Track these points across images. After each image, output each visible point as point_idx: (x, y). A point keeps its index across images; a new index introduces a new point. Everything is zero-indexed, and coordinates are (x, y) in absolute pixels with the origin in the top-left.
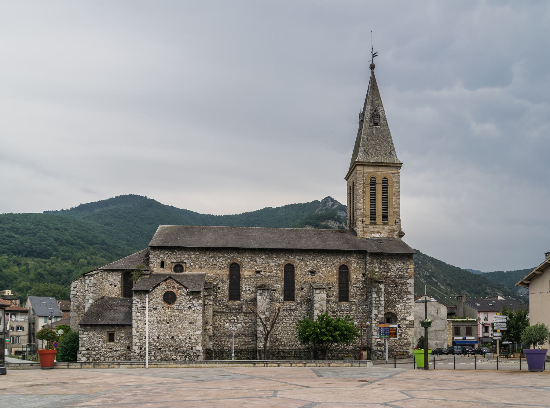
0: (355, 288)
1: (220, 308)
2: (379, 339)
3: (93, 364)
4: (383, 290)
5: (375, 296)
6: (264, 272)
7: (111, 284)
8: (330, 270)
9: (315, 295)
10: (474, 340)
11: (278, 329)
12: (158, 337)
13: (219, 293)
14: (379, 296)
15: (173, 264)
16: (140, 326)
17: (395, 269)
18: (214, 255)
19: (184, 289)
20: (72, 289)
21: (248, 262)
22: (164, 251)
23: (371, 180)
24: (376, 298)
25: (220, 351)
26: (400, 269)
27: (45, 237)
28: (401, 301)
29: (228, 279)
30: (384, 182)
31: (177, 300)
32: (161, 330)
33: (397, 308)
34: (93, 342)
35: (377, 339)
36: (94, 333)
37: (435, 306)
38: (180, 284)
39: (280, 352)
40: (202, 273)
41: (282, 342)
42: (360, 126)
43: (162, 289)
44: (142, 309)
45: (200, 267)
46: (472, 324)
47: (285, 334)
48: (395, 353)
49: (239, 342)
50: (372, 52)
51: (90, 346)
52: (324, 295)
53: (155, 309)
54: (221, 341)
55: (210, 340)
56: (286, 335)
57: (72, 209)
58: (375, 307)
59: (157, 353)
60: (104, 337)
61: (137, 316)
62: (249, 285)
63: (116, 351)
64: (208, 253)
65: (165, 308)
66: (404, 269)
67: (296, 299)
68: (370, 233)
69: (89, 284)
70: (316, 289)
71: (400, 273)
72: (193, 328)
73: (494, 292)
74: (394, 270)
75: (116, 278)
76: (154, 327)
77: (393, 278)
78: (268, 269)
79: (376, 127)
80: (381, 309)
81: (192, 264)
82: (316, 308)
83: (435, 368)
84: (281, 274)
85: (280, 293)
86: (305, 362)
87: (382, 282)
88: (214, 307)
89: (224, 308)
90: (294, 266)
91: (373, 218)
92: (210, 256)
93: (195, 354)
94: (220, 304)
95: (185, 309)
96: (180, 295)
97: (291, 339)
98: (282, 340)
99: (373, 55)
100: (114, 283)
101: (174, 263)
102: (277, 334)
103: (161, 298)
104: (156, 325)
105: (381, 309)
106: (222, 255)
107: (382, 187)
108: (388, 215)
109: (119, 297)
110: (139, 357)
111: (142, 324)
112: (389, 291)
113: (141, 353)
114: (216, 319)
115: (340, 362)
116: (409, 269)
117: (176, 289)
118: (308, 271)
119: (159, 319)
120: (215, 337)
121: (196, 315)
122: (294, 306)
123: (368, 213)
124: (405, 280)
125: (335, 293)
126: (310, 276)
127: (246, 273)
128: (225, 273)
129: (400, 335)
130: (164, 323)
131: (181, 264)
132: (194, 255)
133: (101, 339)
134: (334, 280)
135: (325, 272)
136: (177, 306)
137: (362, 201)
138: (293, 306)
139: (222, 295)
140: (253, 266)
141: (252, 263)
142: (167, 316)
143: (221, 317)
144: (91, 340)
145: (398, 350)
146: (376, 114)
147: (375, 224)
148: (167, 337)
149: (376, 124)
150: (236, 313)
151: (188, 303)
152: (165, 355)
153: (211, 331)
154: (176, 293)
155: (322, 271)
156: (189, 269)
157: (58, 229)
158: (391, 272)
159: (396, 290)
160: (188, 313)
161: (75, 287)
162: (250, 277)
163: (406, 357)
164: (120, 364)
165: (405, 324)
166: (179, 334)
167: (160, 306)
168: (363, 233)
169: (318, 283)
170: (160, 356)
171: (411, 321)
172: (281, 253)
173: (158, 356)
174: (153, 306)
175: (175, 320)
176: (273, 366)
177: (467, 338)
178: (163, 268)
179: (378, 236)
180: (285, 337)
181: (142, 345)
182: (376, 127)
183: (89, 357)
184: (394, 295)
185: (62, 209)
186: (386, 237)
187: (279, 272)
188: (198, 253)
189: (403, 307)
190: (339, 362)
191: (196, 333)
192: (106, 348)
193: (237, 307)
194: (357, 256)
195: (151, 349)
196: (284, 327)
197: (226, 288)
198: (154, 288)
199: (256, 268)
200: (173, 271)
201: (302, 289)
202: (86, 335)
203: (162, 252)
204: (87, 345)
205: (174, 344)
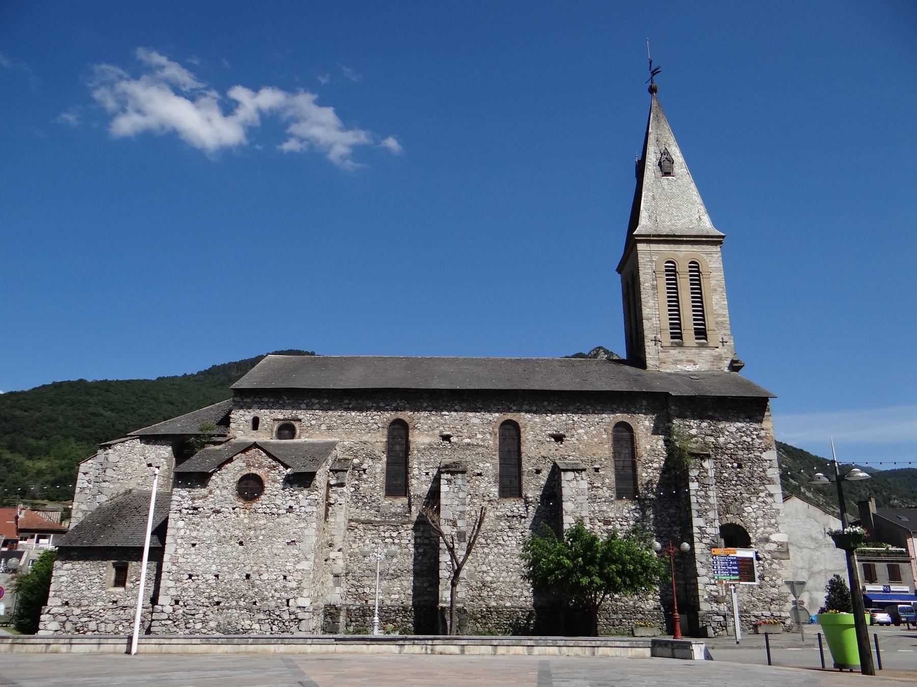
0: (649, 471)
1: (365, 511)
2: (715, 584)
3: (10, 641)
4: (711, 473)
5: (694, 486)
7: (150, 465)
8: (594, 432)
9: (564, 484)
10: (907, 592)
11: (487, 560)
12: (217, 576)
13: (365, 481)
14: (704, 486)
15: (277, 422)
16: (181, 551)
17: (734, 430)
18: (359, 404)
19: (281, 468)
20: (80, 476)
21: (427, 417)
23: (666, 267)
24: (697, 491)
25: (359, 609)
26: (744, 429)
27: (149, 415)
28: (754, 499)
29: (383, 452)
30: (690, 269)
31: (265, 492)
32: (224, 560)
33: (745, 514)
34: (79, 588)
35: (708, 584)
37: (819, 520)
38: (275, 459)
39: (491, 612)
40: (333, 439)
41: (495, 589)
42: (638, 181)
43: (237, 468)
44: (191, 512)
45: (329, 428)
46: (900, 559)
47: (501, 571)
48: (753, 619)
49: (402, 589)
50: (650, 68)
51: (72, 596)
52: (584, 485)
53: (218, 512)
54: (363, 587)
55: (337, 584)
56: (504, 574)
57: (200, 373)
58: (698, 511)
59: (209, 613)
60: (105, 575)
62: (426, 463)
64: (346, 401)
66: (751, 429)
67: (524, 493)
68: (673, 364)
70: (566, 470)
71: (745, 438)
72: (293, 555)
73: (906, 505)
74: (732, 433)
75: (161, 452)
76: (210, 552)
77: (731, 449)
78: (465, 431)
79: (667, 179)
80: (711, 515)
81: (313, 422)
82: (566, 512)
83: (883, 667)
84: (493, 442)
85: (491, 480)
86: (529, 643)
87: (708, 456)
88: (352, 510)
89: (372, 512)
90: (520, 425)
91: (677, 335)
92: (351, 406)
93: (293, 617)
94: (364, 503)
95: (280, 512)
96: (273, 481)
97: (514, 583)
98: (494, 585)
99: (652, 72)
101: (278, 420)
102: (484, 572)
103: (232, 486)
104: (215, 549)
105: (711, 515)
106: (374, 405)
107: (689, 282)
108: (705, 329)
110: (170, 622)
111: (186, 546)
112: (725, 477)
113: (176, 613)
114: (355, 538)
115: (622, 644)
116: (763, 429)
119: (223, 534)
120: (349, 577)
121: (303, 525)
122: (520, 509)
123: (666, 323)
124: (759, 454)
125: (607, 481)
126: (554, 445)
127: (420, 439)
128: (379, 440)
129: (762, 577)
130: (233, 542)
131: (292, 422)
133: (97, 580)
134: (606, 451)
135: (585, 437)
136: (264, 506)
137: (653, 304)
138: (518, 508)
139: (371, 485)
140: (436, 425)
141: (433, 418)
142: (241, 527)
143: (365, 533)
144: (76, 581)
145: (759, 613)
146: (666, 158)
147: (681, 345)
148: (236, 576)
149: (667, 174)
150: (397, 523)
152: (226, 617)
153: (340, 563)
154: (263, 477)
155: (578, 434)
156: (307, 432)
157: (171, 403)
158: (726, 437)
159: (740, 475)
160: (286, 522)
161: (87, 473)
162: (430, 447)
163: (780, 630)
164: (74, 641)
165: (769, 552)
166: (263, 569)
167: (227, 506)
168: (660, 364)
169: (571, 460)
170: (216, 620)
171: (781, 544)
174: (213, 506)
175: (257, 538)
176: (447, 652)
177: (893, 588)
178: (255, 431)
179: (690, 368)
180: (501, 579)
181: (179, 593)
182: (667, 179)
183: (64, 623)
184: (735, 485)
185: (185, 374)
186: (708, 371)
187: (488, 436)
188: (326, 401)
189: (760, 513)
190: (618, 644)
191: (298, 567)
192: (104, 601)
193: (399, 510)
195: (198, 603)
196: (499, 555)
197: (378, 470)
198: (220, 467)
200: (274, 436)
201: (538, 472)
202: (67, 570)
203: (257, 399)
204: (65, 595)
205: (250, 592)
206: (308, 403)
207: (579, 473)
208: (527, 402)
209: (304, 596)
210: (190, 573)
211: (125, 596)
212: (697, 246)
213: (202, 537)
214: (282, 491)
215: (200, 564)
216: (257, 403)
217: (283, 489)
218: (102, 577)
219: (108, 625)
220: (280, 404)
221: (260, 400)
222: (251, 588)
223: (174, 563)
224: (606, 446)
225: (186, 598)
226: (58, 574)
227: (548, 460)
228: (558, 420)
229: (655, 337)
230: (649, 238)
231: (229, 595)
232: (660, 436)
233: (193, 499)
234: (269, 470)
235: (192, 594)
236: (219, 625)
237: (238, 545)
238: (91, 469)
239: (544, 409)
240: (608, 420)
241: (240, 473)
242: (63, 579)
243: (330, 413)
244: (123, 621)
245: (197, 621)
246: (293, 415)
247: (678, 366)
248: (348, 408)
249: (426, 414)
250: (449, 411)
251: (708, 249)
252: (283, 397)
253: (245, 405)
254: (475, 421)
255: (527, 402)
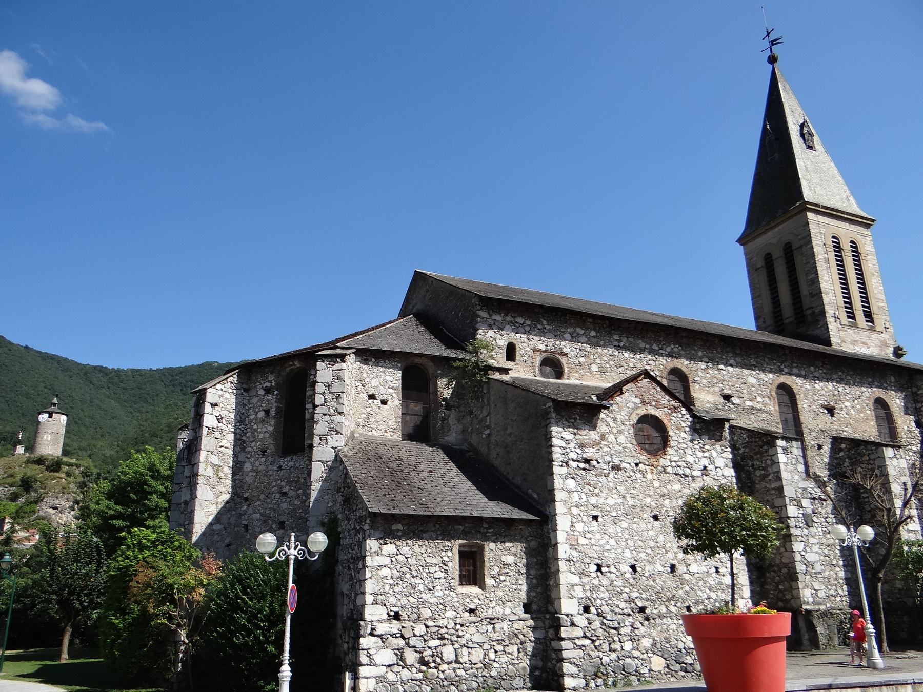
0: (911, 454)
6: (739, 397)
7: (372, 397)
12: (633, 568)
16: (579, 527)
18: (631, 343)
22: (514, 317)
32: (640, 543)
36: (417, 548)
51: (404, 601)
53: (616, 468)
59: (638, 625)
61: (569, 492)
63: (491, 620)
65: (641, 466)
68: (851, 344)
69: (329, 386)
81: (582, 360)
92: (622, 344)
100: (382, 392)
101: (540, 351)
104: (624, 525)
108: (870, 312)
109: (395, 437)
110: (587, 642)
111: (585, 519)
117: (666, 410)
118: (822, 405)
119: (631, 502)
123: (841, 301)
130: (645, 516)
132: (586, 336)
140: (715, 381)
142: (652, 493)
144: (408, 576)
151: (700, 454)
155: (846, 407)
156: (577, 372)
161: (216, 405)
167: (628, 460)
172: (764, 357)
173: (644, 636)
181: (588, 594)
187: (767, 399)
188: (593, 333)
194: (896, 382)
195: (617, 610)
199: (721, 385)
200: (537, 372)
201: (820, 447)
204: (392, 600)
206: (573, 333)
207: (897, 450)
208: (796, 365)
209: (745, 596)
210: (597, 561)
211: (487, 601)
212: (854, 226)
213: (604, 506)
214: (691, 444)
215: (608, 547)
216: (511, 323)
217: (692, 441)
218: (447, 568)
219: (473, 651)
220: (539, 329)
221: (513, 320)
222: (681, 586)
223: (573, 545)
224: (872, 423)
225: (598, 601)
226: (376, 564)
227: (826, 434)
228: (826, 389)
229: (834, 313)
230: (817, 208)
231: (654, 597)
232: (911, 417)
233: (582, 446)
234: (670, 411)
235: (606, 595)
236: (654, 645)
237: (652, 519)
238: (222, 400)
239: (811, 375)
240: (867, 394)
241: (635, 412)
242: (385, 572)
243: (600, 350)
244: (495, 643)
245: (625, 638)
246: (556, 346)
247: (856, 347)
248: (619, 346)
249: (702, 365)
250: (726, 365)
251: (861, 230)
252: (542, 320)
253: (494, 324)
254: (751, 380)
255: (796, 365)
